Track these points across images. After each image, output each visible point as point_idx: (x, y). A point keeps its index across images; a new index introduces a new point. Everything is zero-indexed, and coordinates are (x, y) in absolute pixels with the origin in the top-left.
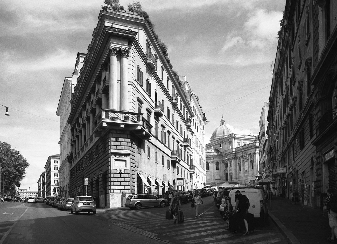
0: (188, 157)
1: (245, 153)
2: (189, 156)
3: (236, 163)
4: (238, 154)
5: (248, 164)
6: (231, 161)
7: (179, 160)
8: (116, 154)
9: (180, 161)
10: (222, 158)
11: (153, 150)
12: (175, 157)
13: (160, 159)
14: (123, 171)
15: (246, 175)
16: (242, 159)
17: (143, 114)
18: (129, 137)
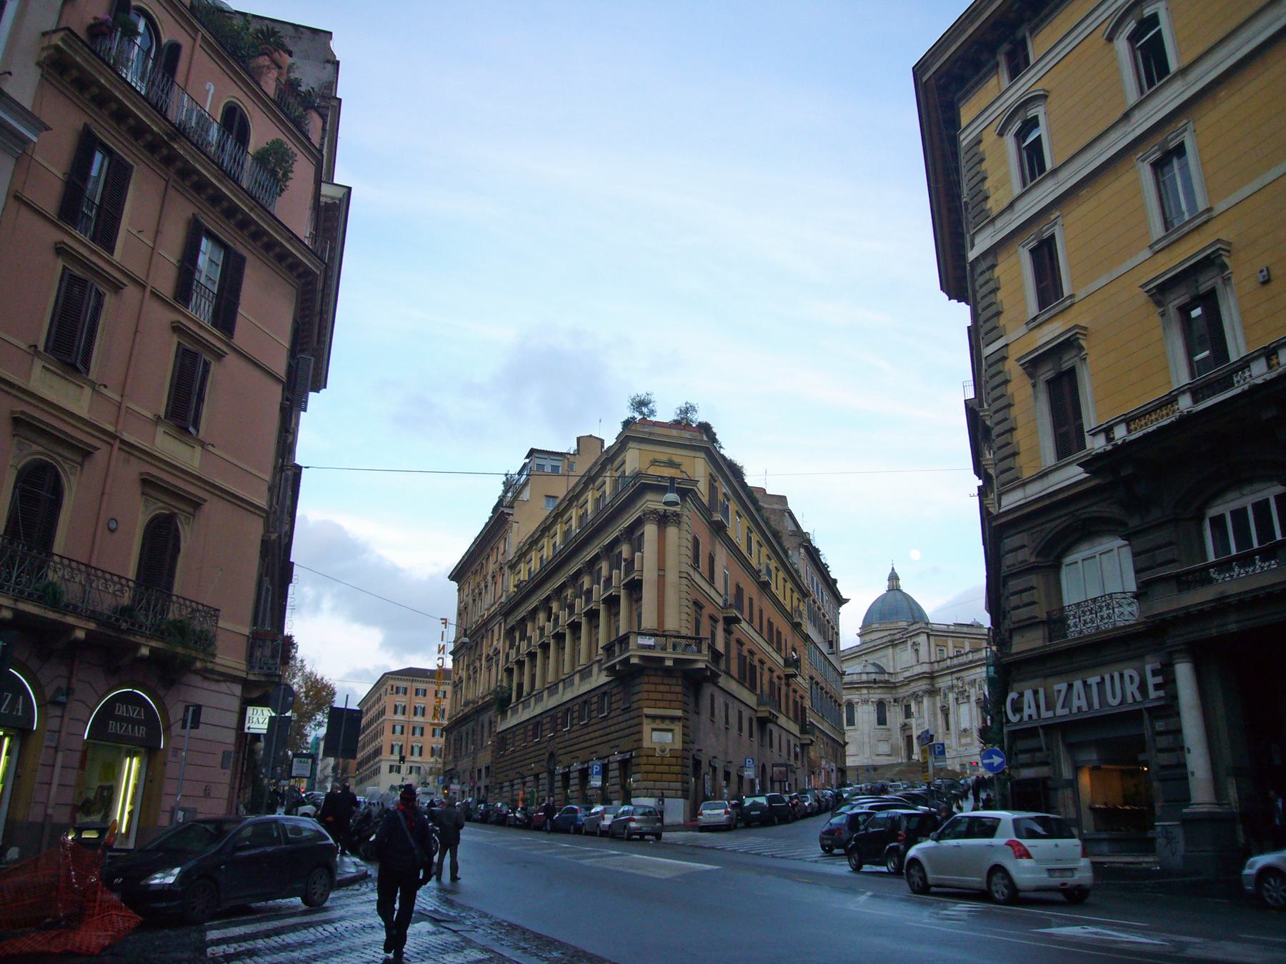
0: (795, 702)
1: (958, 679)
2: (798, 699)
3: (934, 704)
4: (940, 680)
5: (970, 709)
6: (919, 699)
7: (774, 715)
8: (654, 718)
9: (777, 717)
10: (894, 692)
11: (720, 700)
12: (764, 711)
13: (733, 719)
14: (668, 750)
15: (963, 741)
16: (951, 696)
17: (48, 129)
18: (680, 683)
